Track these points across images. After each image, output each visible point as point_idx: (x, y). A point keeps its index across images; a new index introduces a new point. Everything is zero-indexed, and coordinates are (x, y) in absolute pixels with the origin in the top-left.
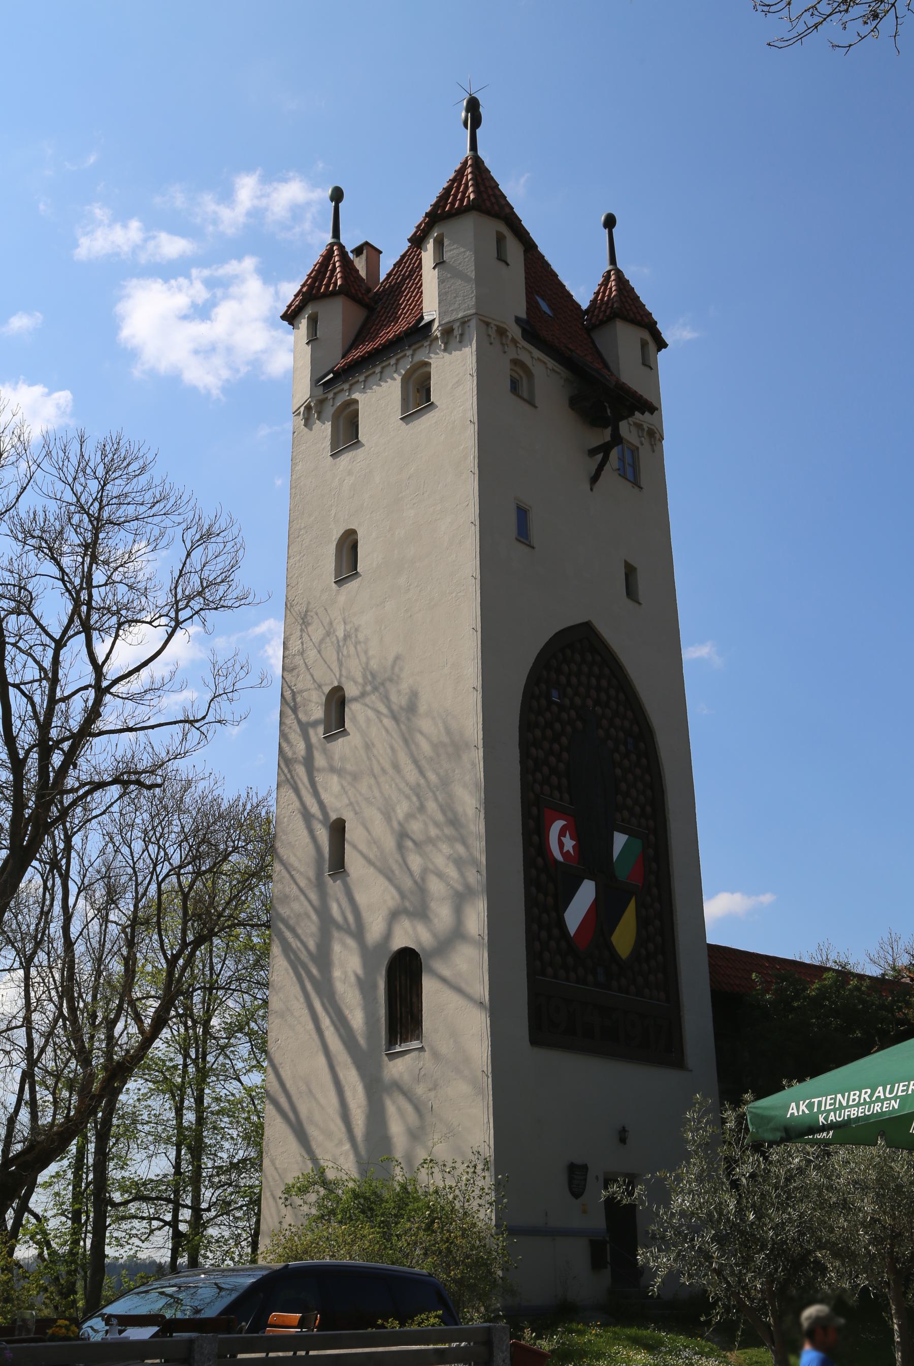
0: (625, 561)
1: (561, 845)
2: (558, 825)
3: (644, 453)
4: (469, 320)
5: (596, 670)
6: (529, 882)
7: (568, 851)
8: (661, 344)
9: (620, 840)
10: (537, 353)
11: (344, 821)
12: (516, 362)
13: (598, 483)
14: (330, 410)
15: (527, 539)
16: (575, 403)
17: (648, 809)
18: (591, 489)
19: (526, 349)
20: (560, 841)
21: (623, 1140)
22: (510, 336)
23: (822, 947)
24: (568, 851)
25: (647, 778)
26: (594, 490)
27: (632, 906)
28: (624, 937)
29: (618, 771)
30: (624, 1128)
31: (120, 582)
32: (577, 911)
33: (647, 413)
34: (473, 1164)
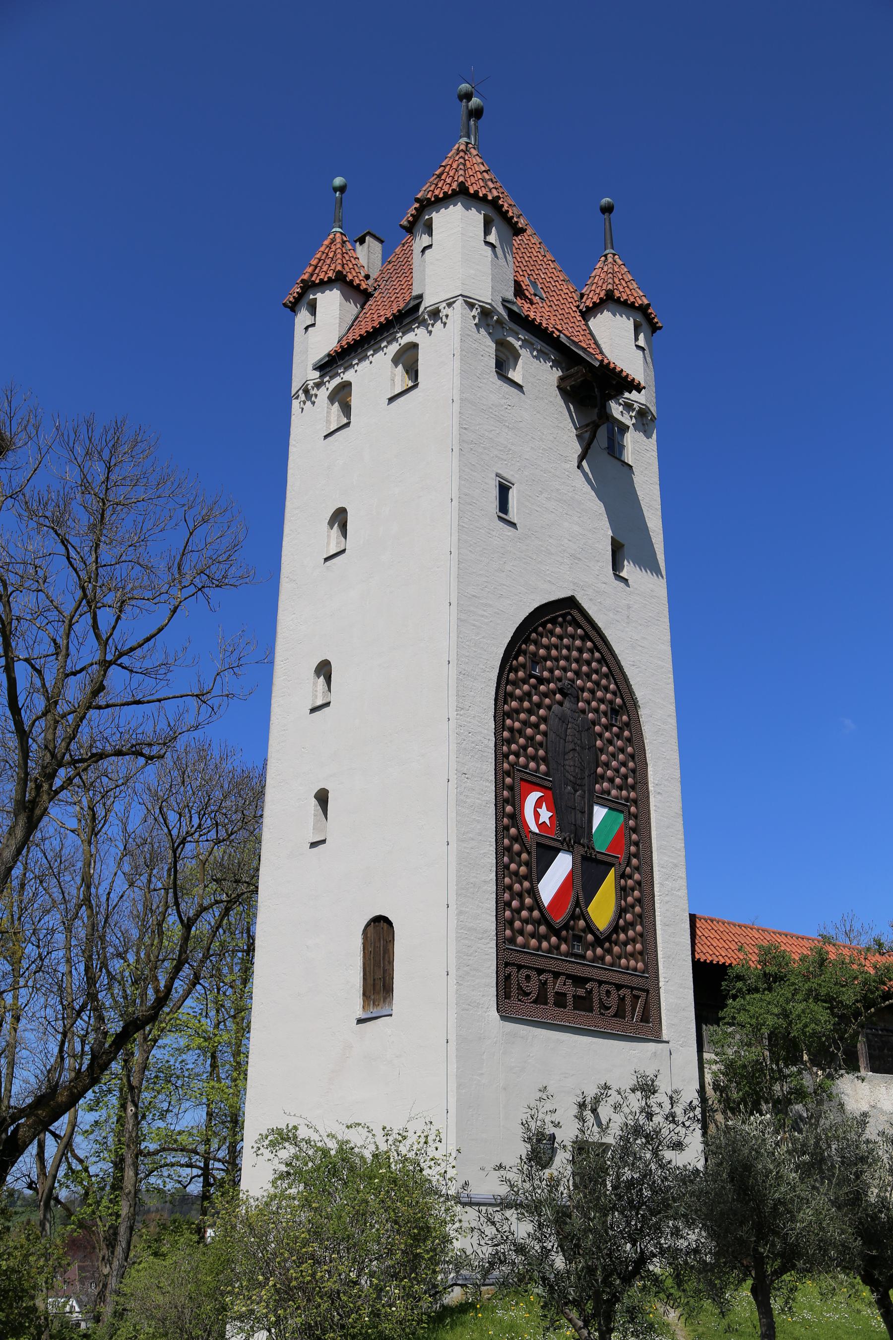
1: (537, 815)
2: (534, 796)
4: (454, 302)
6: (501, 850)
9: (599, 813)
11: (328, 791)
20: (535, 812)
23: (846, 918)
27: (611, 874)
28: (602, 909)
32: (549, 886)
33: (634, 392)
34: (425, 1134)
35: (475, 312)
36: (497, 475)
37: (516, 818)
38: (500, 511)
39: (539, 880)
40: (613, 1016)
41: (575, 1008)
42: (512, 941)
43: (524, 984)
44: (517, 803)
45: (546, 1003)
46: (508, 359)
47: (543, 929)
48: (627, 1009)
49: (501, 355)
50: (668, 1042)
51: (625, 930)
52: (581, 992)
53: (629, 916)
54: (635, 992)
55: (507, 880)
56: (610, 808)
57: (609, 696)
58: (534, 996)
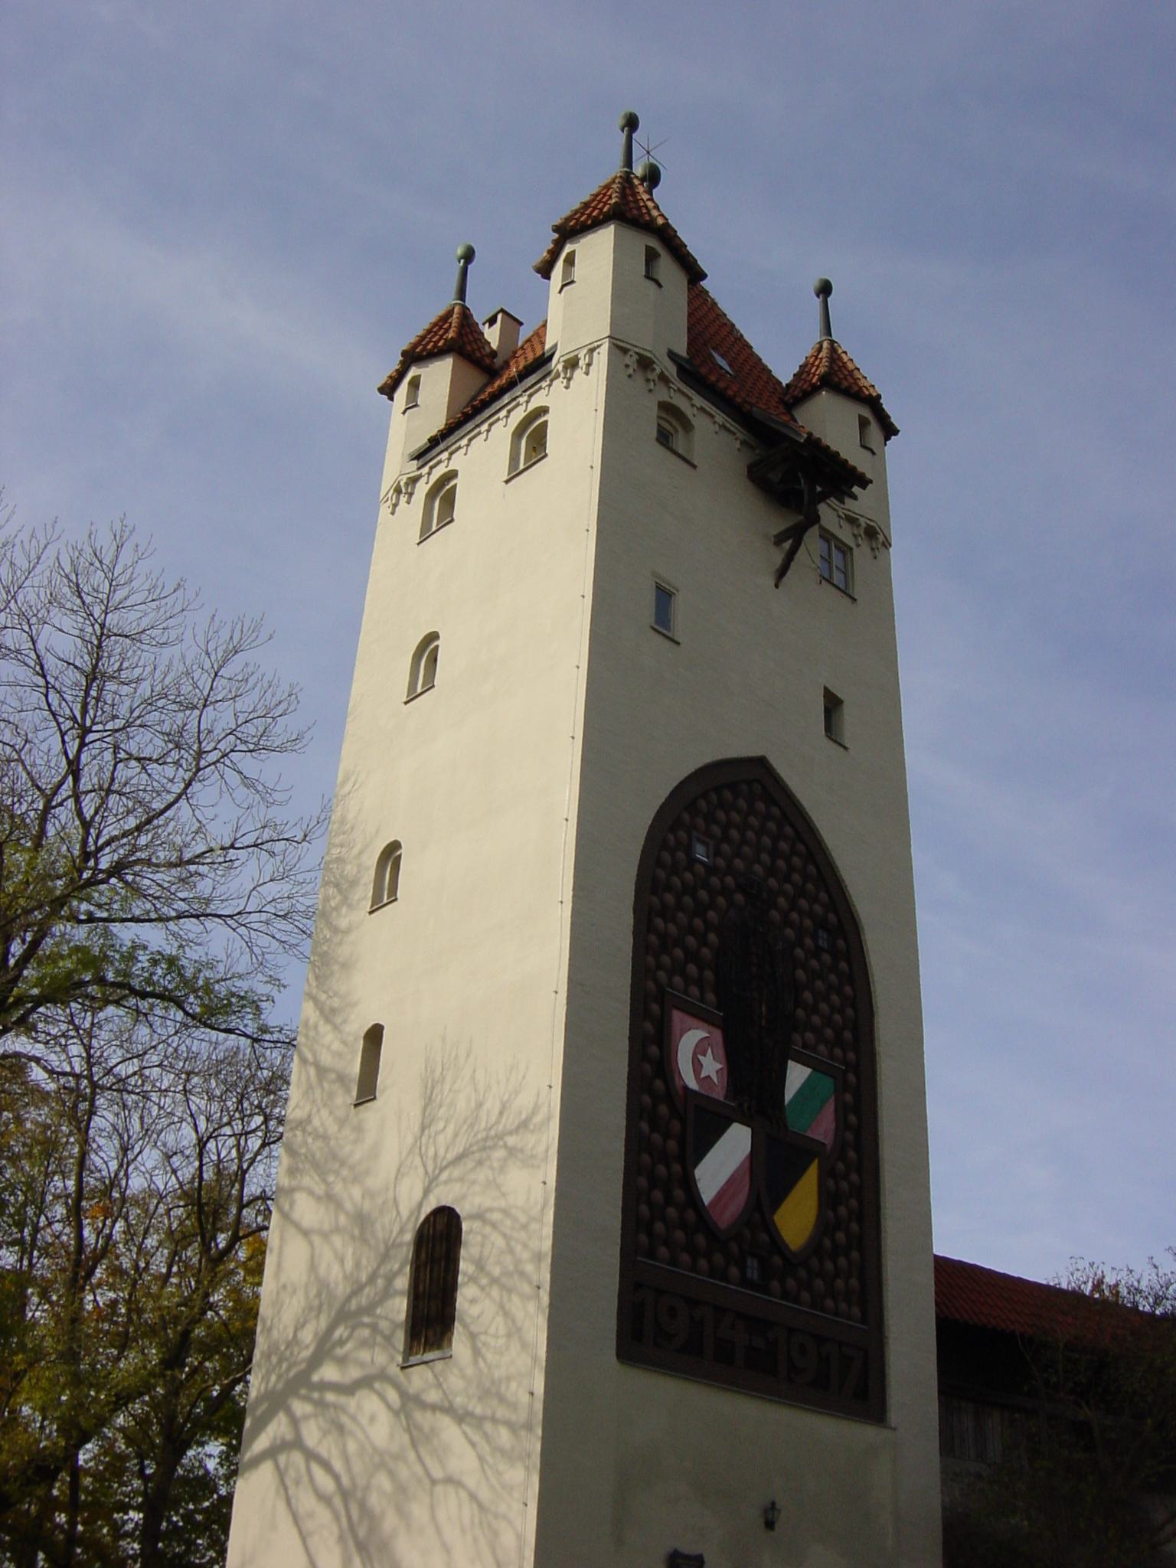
0: (826, 689)
1: (697, 1066)
3: (861, 554)
5: (772, 826)
7: (708, 1077)
8: (889, 430)
10: (699, 401)
12: (666, 407)
13: (785, 579)
14: (422, 489)
15: (669, 630)
16: (757, 476)
17: (848, 1035)
18: (777, 586)
19: (683, 393)
20: (697, 1058)
21: (770, 1525)
22: (658, 371)
24: (708, 1077)
25: (848, 989)
28: (797, 1218)
29: (800, 974)
30: (773, 1504)
32: (723, 1162)
35: (628, 360)
36: (654, 574)
37: (665, 1066)
38: (657, 622)
39: (449, 314)
42: (651, 1254)
46: (676, 431)
47: (701, 1240)
48: (852, 1384)
49: (666, 425)
50: (895, 1429)
53: (840, 1236)
55: (646, 1158)
56: (814, 1069)
57: (817, 908)
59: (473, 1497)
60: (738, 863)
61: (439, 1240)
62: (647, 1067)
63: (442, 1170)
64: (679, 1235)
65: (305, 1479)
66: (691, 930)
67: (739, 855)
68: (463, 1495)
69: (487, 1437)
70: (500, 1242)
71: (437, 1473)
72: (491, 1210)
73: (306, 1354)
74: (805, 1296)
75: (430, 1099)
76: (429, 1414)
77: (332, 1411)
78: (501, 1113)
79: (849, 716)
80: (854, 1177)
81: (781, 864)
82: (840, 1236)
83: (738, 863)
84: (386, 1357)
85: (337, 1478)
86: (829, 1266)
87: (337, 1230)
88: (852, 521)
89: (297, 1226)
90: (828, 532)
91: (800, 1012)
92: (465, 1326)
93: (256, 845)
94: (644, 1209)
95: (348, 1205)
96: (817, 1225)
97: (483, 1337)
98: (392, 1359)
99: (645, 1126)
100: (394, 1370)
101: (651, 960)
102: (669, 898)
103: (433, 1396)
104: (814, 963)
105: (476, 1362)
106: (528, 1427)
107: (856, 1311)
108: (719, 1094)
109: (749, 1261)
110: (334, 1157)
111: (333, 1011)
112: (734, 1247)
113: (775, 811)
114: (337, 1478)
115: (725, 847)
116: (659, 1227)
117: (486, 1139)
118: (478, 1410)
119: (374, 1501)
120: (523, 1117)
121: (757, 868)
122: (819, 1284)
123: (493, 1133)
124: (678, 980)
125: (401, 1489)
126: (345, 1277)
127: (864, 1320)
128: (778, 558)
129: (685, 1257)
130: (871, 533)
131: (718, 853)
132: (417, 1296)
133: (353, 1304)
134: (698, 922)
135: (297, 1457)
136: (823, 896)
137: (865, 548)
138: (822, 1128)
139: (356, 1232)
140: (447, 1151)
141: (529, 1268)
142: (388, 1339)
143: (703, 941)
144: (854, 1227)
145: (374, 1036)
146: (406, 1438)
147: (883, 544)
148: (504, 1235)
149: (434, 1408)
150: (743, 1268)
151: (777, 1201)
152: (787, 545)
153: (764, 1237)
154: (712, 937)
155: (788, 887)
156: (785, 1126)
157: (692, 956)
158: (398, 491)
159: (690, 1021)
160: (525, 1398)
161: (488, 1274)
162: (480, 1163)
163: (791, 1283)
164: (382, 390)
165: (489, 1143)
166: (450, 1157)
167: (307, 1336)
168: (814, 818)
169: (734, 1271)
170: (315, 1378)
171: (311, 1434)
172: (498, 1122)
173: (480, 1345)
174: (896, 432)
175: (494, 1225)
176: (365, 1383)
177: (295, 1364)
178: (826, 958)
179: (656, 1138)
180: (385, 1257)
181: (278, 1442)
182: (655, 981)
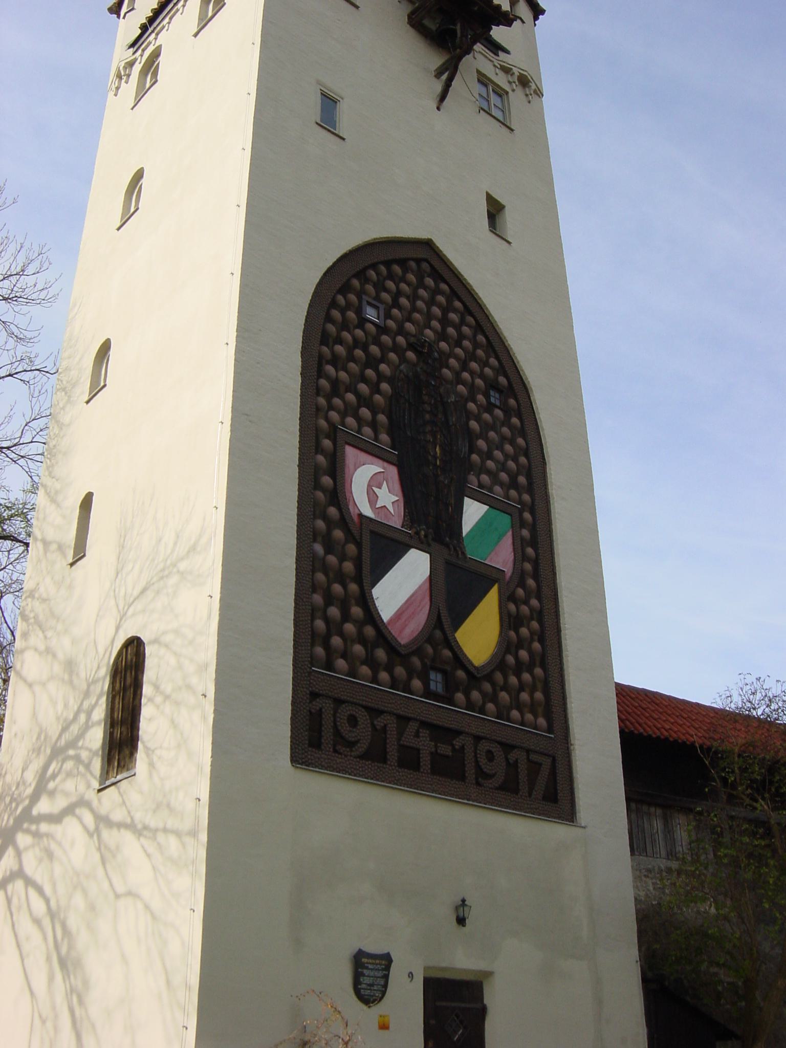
1: (373, 498)
3: (517, 97)
5: (441, 299)
17: (522, 480)
18: (438, 109)
20: (372, 489)
21: (461, 921)
26: (442, 108)
28: (479, 635)
29: (474, 424)
30: (463, 901)
31: (30, 685)
32: (401, 587)
36: (319, 83)
37: (338, 495)
40: (497, 789)
41: (545, 798)
43: (345, 728)
44: (336, 469)
45: (384, 760)
48: (545, 789)
50: (584, 827)
51: (519, 668)
52: (445, 750)
53: (523, 654)
54: (533, 757)
55: (320, 577)
58: (362, 748)
59: (147, 907)
60: (409, 326)
61: (129, 667)
62: (320, 495)
63: (130, 606)
64: (358, 649)
65: (25, 905)
66: (364, 379)
67: (409, 319)
68: (140, 906)
69: (159, 846)
70: (173, 661)
71: (120, 889)
72: (165, 633)
73: (29, 791)
74: (490, 706)
75: (123, 547)
76: (115, 831)
77: (45, 839)
78: (175, 544)
79: (510, 219)
80: (534, 602)
81: (451, 331)
82: (523, 654)
83: (409, 326)
84: (80, 781)
85: (47, 901)
86: (513, 680)
87: (52, 678)
88: (507, 70)
89: (25, 681)
90: (484, 75)
91: (475, 457)
92: (143, 743)
93: (10, 375)
94: (320, 624)
95: (61, 656)
96: (499, 643)
97: (158, 752)
98: (89, 786)
99: (319, 548)
100: (91, 795)
101: (322, 401)
102: (339, 349)
103: (118, 815)
104: (486, 416)
105: (151, 776)
106: (193, 833)
107: (542, 721)
108: (396, 522)
109: (433, 675)
110: (52, 614)
111: (57, 492)
112: (416, 661)
113: (444, 286)
114: (47, 901)
115: (395, 311)
116: (336, 641)
117: (163, 570)
118: (153, 824)
119: (73, 922)
120: (192, 542)
121: (428, 332)
122: (504, 696)
123: (169, 562)
124: (350, 421)
125: (92, 907)
126: (58, 718)
127: (550, 730)
128: (438, 87)
129: (365, 670)
130: (524, 81)
131: (388, 316)
132: (112, 723)
133: (63, 742)
134: (370, 372)
135: (19, 884)
136: (493, 361)
137: (519, 91)
138: (502, 557)
139: (66, 677)
140: (133, 589)
141: (194, 680)
142: (88, 766)
143: (376, 389)
144: (536, 646)
145: (87, 503)
146: (97, 856)
147: (535, 92)
148: (175, 654)
149: (120, 825)
150: (426, 683)
151: (459, 618)
152: (444, 77)
153: (447, 653)
154: (385, 386)
155: (458, 351)
156: (463, 553)
157: (363, 401)
158: (120, 77)
159: (363, 456)
160: (190, 805)
161: (162, 693)
162: (158, 592)
163: (475, 695)
164: (111, 10)
165: (166, 572)
166: (136, 592)
167: (31, 777)
168: (481, 295)
169: (417, 684)
170: (35, 812)
171: (31, 864)
172: (173, 551)
173: (155, 759)
174: (542, 12)
175: (167, 646)
176: (69, 810)
177: (23, 800)
178: (498, 413)
179: (332, 559)
180: (87, 694)
181: (8, 873)
182: (327, 419)
